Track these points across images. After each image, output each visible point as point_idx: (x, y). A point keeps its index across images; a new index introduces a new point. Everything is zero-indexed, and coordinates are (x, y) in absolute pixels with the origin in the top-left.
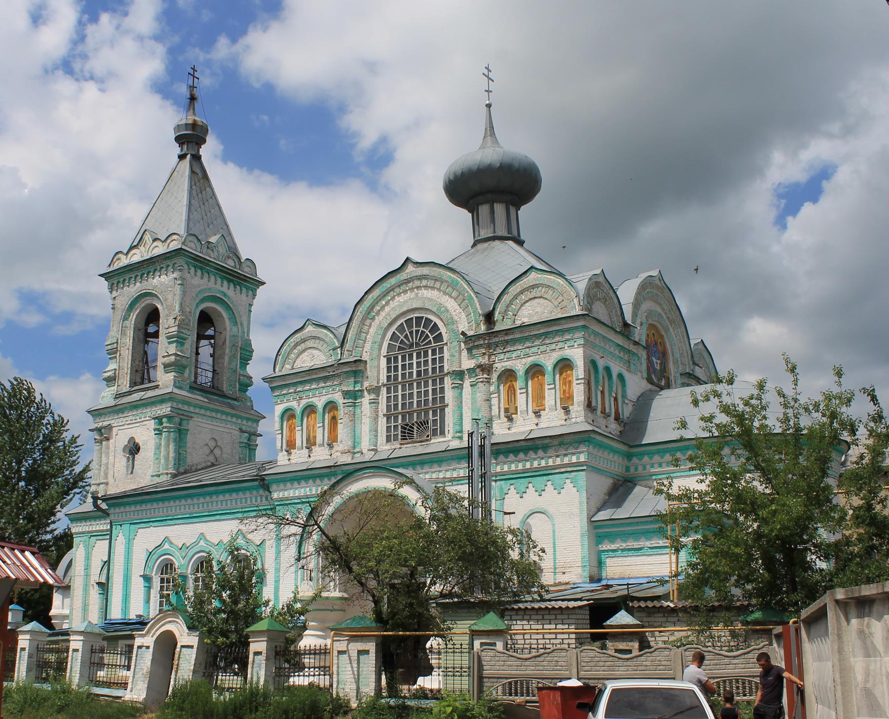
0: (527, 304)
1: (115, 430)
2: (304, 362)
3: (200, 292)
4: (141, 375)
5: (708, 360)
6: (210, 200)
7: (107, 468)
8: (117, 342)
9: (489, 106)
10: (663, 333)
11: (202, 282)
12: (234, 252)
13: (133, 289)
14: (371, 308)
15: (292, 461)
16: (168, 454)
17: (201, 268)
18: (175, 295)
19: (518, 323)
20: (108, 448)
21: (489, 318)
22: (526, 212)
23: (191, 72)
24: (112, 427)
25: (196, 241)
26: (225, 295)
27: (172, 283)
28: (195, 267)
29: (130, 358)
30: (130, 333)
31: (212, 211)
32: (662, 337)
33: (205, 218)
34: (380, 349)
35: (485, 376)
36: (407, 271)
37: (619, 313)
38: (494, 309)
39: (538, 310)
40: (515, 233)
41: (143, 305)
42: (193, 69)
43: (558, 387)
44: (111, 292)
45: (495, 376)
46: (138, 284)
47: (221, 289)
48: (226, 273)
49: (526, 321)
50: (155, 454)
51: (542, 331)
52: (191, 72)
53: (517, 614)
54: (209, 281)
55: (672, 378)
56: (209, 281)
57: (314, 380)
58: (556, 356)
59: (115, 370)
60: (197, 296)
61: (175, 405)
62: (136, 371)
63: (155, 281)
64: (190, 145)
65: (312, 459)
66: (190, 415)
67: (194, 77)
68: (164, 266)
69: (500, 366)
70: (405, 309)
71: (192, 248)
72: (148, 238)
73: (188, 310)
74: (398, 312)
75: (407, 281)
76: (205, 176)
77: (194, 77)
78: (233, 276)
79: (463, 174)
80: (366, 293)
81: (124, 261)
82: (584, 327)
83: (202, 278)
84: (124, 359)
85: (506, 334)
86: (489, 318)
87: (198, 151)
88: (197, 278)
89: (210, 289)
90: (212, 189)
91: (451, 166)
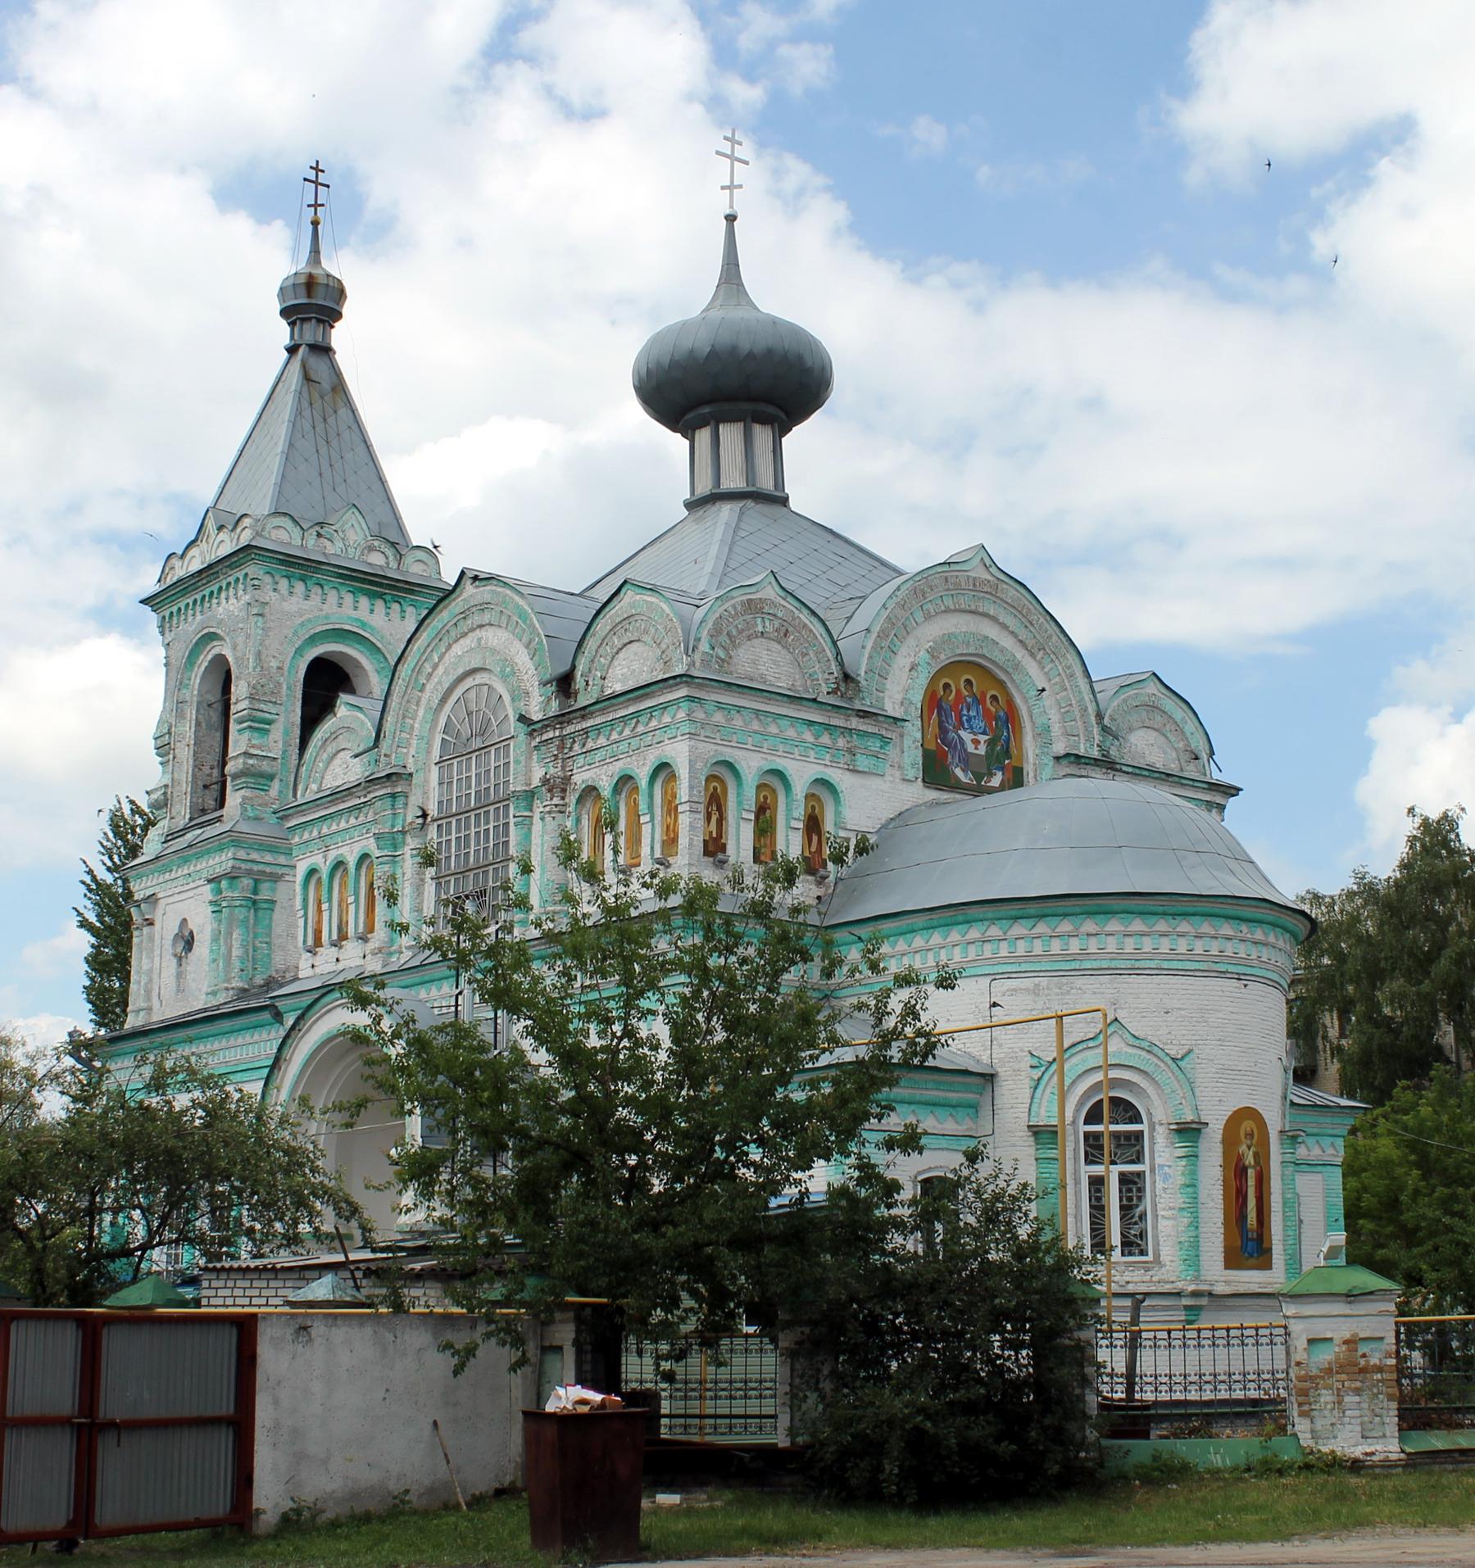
0: (621, 655)
1: (162, 903)
2: (335, 778)
3: (302, 624)
4: (215, 794)
5: (1179, 713)
6: (346, 435)
7: (151, 980)
8: (169, 733)
9: (731, 219)
10: (1003, 677)
11: (306, 605)
12: (392, 535)
13: (191, 627)
14: (418, 670)
15: (318, 970)
16: (230, 951)
17: (303, 579)
18: (248, 636)
19: (608, 692)
20: (151, 939)
21: (564, 684)
22: (800, 441)
23: (312, 175)
24: (157, 900)
25: (288, 524)
26: (364, 625)
27: (243, 614)
28: (288, 577)
29: (191, 762)
30: (191, 713)
31: (348, 456)
32: (1001, 684)
33: (327, 472)
34: (429, 752)
35: (556, 801)
36: (465, 595)
37: (830, 654)
38: (573, 667)
39: (636, 666)
40: (766, 483)
41: (210, 657)
42: (317, 169)
43: (658, 818)
44: (162, 633)
45: (572, 799)
46: (199, 617)
47: (354, 614)
48: (363, 581)
49: (619, 688)
50: (212, 951)
51: (631, 710)
52: (312, 175)
53: (276, 1279)
54: (324, 601)
55: (1029, 769)
56: (324, 601)
57: (340, 813)
58: (651, 759)
59: (166, 786)
60: (295, 633)
61: (242, 854)
62: (206, 787)
63: (221, 609)
64: (306, 326)
65: (340, 966)
66: (280, 871)
67: (316, 183)
68: (231, 579)
69: (580, 778)
70: (460, 671)
71: (285, 537)
72: (211, 525)
73: (274, 664)
74: (452, 678)
75: (465, 614)
76: (339, 386)
77: (316, 183)
78: (381, 585)
79: (770, 352)
80: (409, 641)
81: (181, 570)
82: (690, 698)
83: (307, 597)
84: (181, 764)
85: (583, 717)
86: (564, 684)
87: (326, 336)
88: (294, 599)
89: (327, 617)
90: (353, 411)
91: (638, 360)
